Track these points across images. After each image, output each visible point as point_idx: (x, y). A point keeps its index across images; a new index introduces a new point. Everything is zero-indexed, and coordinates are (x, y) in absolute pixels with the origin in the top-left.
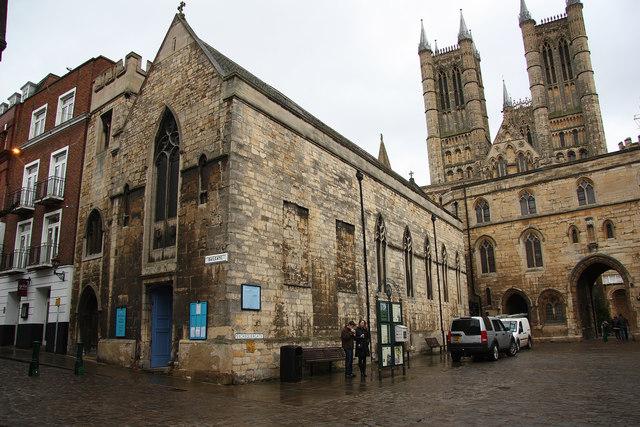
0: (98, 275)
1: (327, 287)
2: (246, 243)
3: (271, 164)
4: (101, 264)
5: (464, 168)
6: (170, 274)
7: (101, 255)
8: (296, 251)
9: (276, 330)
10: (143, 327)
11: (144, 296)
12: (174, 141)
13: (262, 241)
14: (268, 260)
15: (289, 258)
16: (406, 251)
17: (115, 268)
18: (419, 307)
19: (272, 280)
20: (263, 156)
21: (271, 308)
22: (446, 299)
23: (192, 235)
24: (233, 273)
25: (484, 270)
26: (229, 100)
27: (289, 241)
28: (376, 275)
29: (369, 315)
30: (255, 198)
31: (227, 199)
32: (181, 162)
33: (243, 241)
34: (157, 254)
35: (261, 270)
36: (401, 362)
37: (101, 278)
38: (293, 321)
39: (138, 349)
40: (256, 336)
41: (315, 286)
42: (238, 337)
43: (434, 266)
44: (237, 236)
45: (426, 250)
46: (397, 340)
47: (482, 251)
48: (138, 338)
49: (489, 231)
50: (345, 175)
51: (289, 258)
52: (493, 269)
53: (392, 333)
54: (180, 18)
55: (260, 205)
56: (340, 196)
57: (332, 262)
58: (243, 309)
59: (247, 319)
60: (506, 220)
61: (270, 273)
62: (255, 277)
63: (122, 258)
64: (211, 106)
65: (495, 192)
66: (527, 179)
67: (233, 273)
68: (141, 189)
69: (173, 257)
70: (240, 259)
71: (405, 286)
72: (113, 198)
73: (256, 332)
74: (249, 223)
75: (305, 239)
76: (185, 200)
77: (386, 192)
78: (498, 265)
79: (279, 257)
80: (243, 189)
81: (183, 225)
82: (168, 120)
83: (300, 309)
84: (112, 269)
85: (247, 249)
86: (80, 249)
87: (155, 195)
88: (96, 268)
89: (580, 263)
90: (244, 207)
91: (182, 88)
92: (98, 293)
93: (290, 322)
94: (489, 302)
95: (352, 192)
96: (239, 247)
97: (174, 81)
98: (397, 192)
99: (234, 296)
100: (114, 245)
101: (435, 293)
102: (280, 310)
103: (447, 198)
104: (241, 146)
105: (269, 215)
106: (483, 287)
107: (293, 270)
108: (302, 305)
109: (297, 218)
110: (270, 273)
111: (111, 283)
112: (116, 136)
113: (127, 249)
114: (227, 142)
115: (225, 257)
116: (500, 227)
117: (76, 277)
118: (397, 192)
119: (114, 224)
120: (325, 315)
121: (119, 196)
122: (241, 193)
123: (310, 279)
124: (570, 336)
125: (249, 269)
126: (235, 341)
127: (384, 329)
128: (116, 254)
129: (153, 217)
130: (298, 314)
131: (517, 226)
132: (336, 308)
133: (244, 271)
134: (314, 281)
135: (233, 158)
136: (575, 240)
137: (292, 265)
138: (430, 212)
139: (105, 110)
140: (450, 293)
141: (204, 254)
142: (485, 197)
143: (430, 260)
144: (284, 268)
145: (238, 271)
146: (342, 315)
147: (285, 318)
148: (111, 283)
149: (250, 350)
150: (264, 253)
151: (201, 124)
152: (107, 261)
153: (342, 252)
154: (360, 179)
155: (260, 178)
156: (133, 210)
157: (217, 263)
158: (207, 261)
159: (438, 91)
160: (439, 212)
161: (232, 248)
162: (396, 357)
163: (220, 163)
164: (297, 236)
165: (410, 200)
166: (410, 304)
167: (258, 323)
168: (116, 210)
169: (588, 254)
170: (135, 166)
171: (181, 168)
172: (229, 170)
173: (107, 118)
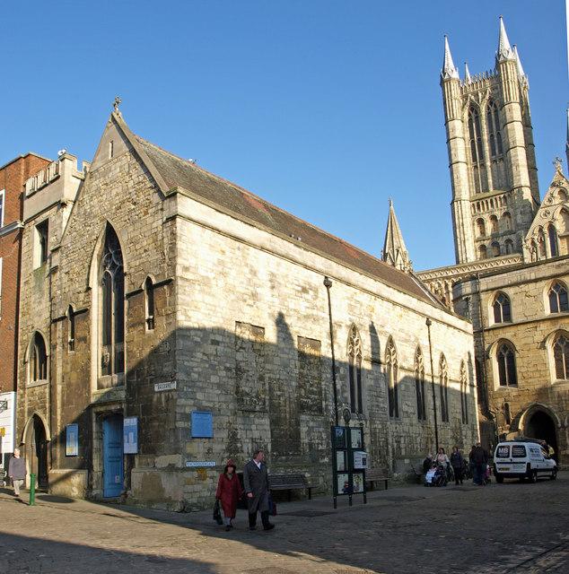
0: (45, 402)
1: (287, 410)
2: (196, 369)
3: (221, 283)
4: (47, 390)
5: (501, 241)
6: (120, 402)
8: (250, 373)
9: (228, 457)
13: (212, 367)
14: (219, 386)
15: (243, 382)
16: (462, 383)
17: (63, 396)
18: (406, 428)
19: (224, 406)
20: (211, 275)
21: (224, 434)
24: (182, 401)
25: (503, 382)
26: (173, 218)
27: (242, 364)
28: (348, 395)
35: (210, 396)
36: (361, 489)
40: (208, 464)
41: (273, 410)
42: (188, 465)
44: (186, 363)
45: (417, 361)
46: (356, 467)
47: (500, 359)
48: (90, 468)
49: (508, 334)
50: (309, 284)
52: (513, 381)
53: (350, 459)
56: (303, 309)
57: (294, 384)
59: (197, 448)
60: (530, 319)
62: (205, 404)
63: (69, 385)
64: (155, 225)
65: (517, 284)
66: (559, 266)
68: (85, 312)
70: (190, 387)
71: (387, 406)
72: (55, 321)
75: (261, 360)
76: (133, 326)
77: (364, 298)
78: (519, 376)
79: (232, 382)
81: (131, 351)
82: (111, 237)
83: (256, 434)
85: (196, 376)
88: (42, 397)
91: (123, 202)
92: (46, 422)
93: (245, 448)
95: (319, 303)
96: (188, 374)
97: (114, 192)
98: (377, 296)
99: (180, 424)
100: (59, 371)
102: (233, 438)
104: (186, 269)
106: (500, 402)
108: (261, 429)
111: (59, 411)
112: (54, 251)
114: (173, 267)
115: (174, 386)
116: (522, 328)
118: (377, 296)
119: (59, 348)
120: (286, 441)
123: (267, 403)
125: (199, 396)
127: (340, 456)
130: (253, 440)
131: (543, 326)
132: (298, 433)
134: (271, 405)
135: (180, 282)
137: (247, 390)
138: (423, 315)
139: (40, 219)
140: (451, 410)
142: (505, 290)
144: (237, 393)
145: (187, 399)
146: (305, 440)
147: (239, 445)
150: (214, 379)
151: (145, 243)
152: (52, 387)
153: (305, 372)
154: (328, 285)
155: (208, 299)
156: (79, 334)
157: (165, 391)
158: (156, 389)
159: (467, 135)
160: (437, 313)
161: (180, 376)
162: (355, 484)
165: (395, 304)
167: (209, 451)
168: (59, 334)
173: (43, 228)
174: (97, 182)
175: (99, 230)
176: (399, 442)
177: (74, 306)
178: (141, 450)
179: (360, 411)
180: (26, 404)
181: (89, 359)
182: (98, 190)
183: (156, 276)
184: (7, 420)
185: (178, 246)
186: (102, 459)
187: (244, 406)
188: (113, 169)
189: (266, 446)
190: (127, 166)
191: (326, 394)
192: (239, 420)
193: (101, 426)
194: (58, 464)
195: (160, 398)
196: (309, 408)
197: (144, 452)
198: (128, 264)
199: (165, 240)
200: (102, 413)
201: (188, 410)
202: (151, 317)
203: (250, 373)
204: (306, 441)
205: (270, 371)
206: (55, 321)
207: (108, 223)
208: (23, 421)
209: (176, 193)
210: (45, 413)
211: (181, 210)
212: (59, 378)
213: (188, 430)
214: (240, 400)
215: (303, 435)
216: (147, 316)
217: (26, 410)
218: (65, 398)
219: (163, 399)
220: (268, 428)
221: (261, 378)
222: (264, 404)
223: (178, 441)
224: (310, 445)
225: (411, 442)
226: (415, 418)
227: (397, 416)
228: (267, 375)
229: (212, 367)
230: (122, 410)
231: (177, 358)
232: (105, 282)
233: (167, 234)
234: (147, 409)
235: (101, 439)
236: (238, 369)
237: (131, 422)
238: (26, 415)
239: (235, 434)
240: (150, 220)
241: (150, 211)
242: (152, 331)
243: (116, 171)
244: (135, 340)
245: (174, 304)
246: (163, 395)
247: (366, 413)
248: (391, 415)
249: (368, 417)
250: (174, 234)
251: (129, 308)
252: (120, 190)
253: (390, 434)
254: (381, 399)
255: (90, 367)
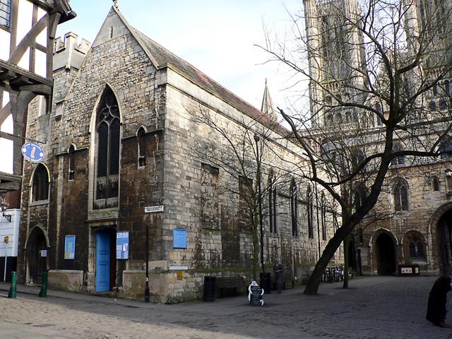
0: (46, 218)
3: (192, 135)
6: (114, 220)
7: (47, 201)
8: (210, 201)
9: (196, 263)
10: (89, 260)
11: (90, 236)
12: (113, 114)
19: (194, 225)
22: (324, 238)
23: (132, 190)
24: (168, 221)
26: (163, 86)
29: (262, 250)
30: (182, 162)
31: (161, 163)
32: (121, 132)
33: (174, 196)
34: (101, 202)
35: (185, 218)
37: (48, 220)
38: (207, 256)
39: (86, 277)
43: (315, 211)
44: (170, 192)
48: (86, 270)
51: (205, 207)
54: (114, 11)
55: (185, 168)
57: (236, 210)
58: (174, 248)
61: (193, 219)
62: (182, 223)
63: (68, 205)
64: (147, 90)
67: (168, 221)
68: (85, 152)
69: (115, 206)
70: (173, 210)
73: (183, 264)
74: (178, 182)
76: (125, 163)
80: (174, 156)
81: (125, 182)
82: (108, 97)
83: (213, 247)
84: (59, 214)
85: (176, 202)
86: (27, 195)
87: (97, 156)
89: (439, 209)
90: (175, 170)
94: (361, 240)
96: (172, 201)
97: (113, 63)
100: (60, 194)
101: (316, 233)
102: (199, 250)
103: (349, 26)
104: (172, 123)
105: (191, 175)
107: (208, 217)
108: (214, 243)
109: (211, 176)
110: (193, 219)
111: (58, 225)
113: (73, 198)
114: (163, 121)
117: (23, 219)
119: (60, 177)
120: (231, 250)
121: (64, 155)
122: (173, 159)
124: (429, 271)
125: (178, 217)
126: (169, 271)
128: (63, 202)
129: (96, 174)
132: (238, 246)
133: (175, 219)
134: (222, 225)
135: (167, 132)
136: (436, 189)
137: (207, 213)
141: (143, 205)
143: (312, 205)
144: (201, 216)
147: (203, 254)
148: (58, 225)
149: (180, 278)
150: (188, 205)
152: (53, 207)
158: (146, 211)
161: (167, 202)
163: (156, 136)
164: (210, 189)
166: (295, 242)
169: (446, 201)
170: (77, 132)
171: (121, 137)
172: (164, 142)
174: (98, 55)
175: (98, 90)
176: (297, 254)
177: (75, 146)
178: (131, 257)
179: (275, 232)
180: (28, 219)
181: (88, 187)
182: (99, 61)
183: (148, 127)
184: (13, 231)
185: (167, 106)
186: (95, 263)
187: (206, 225)
188: (112, 46)
189: (219, 255)
190: (124, 45)
191: (397, 224)
192: (203, 236)
193: (95, 237)
194: (57, 265)
195: (148, 218)
196: (245, 228)
197: (133, 258)
198: (124, 117)
199: (156, 101)
200: (96, 227)
201: (171, 228)
202: (143, 157)
203: (210, 201)
204: (243, 252)
205: (222, 201)
206: (58, 157)
207: (107, 85)
208: (25, 232)
209: (167, 67)
210: (45, 226)
211: (169, 81)
212: (59, 200)
213: (171, 242)
214: (203, 221)
215: (241, 248)
216: (139, 157)
217: (28, 223)
218: (64, 215)
219: (152, 219)
220: (220, 242)
221: (216, 205)
222: (218, 223)
223: (165, 251)
224: (246, 255)
225: (305, 255)
226: (307, 236)
227: (297, 235)
228: (220, 203)
229: (187, 196)
230: (115, 225)
231: (164, 188)
232: (101, 129)
233: (158, 96)
234: (137, 226)
235: (94, 247)
236: (202, 198)
237: (123, 236)
238: (28, 227)
239: (200, 246)
240: (143, 86)
241: (143, 79)
242: (144, 167)
243: (115, 48)
244: (128, 173)
245: (162, 148)
246: (151, 216)
247: (279, 232)
248: (293, 235)
249: (279, 236)
250: (163, 97)
251: (123, 150)
252: (118, 62)
253: (293, 248)
254: (287, 223)
255: (88, 192)
